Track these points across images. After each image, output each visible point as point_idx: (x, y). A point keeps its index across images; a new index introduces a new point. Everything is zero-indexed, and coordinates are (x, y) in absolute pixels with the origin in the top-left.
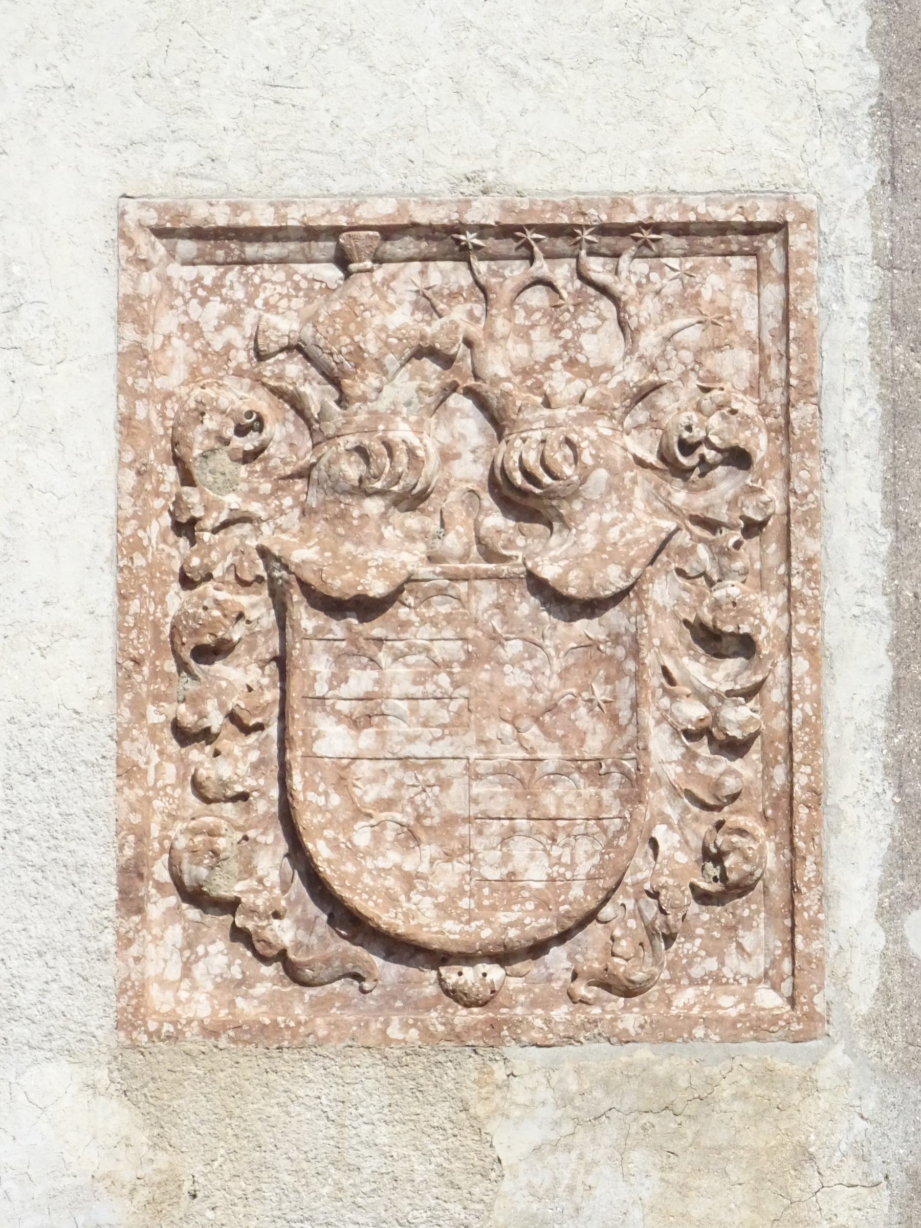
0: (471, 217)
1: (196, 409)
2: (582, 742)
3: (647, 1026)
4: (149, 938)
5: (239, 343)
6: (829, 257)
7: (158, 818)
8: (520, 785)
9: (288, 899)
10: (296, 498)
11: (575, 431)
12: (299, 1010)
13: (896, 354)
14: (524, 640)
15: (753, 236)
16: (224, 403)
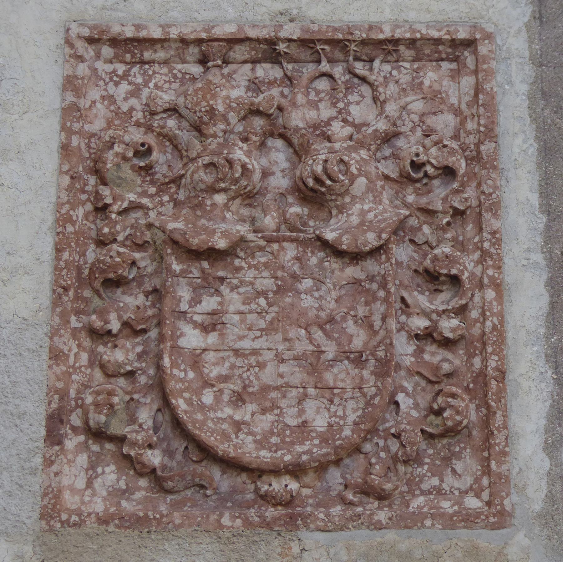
0: (283, 34)
1: (109, 142)
2: (350, 342)
3: (394, 519)
4: (65, 461)
5: (138, 107)
6: (503, 59)
7: (75, 386)
8: (311, 368)
9: (158, 438)
10: (171, 197)
11: (346, 155)
12: (163, 508)
13: (545, 114)
14: (314, 279)
15: (458, 49)
16: (127, 138)
